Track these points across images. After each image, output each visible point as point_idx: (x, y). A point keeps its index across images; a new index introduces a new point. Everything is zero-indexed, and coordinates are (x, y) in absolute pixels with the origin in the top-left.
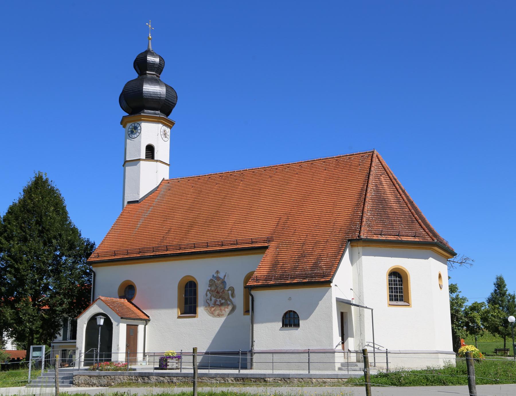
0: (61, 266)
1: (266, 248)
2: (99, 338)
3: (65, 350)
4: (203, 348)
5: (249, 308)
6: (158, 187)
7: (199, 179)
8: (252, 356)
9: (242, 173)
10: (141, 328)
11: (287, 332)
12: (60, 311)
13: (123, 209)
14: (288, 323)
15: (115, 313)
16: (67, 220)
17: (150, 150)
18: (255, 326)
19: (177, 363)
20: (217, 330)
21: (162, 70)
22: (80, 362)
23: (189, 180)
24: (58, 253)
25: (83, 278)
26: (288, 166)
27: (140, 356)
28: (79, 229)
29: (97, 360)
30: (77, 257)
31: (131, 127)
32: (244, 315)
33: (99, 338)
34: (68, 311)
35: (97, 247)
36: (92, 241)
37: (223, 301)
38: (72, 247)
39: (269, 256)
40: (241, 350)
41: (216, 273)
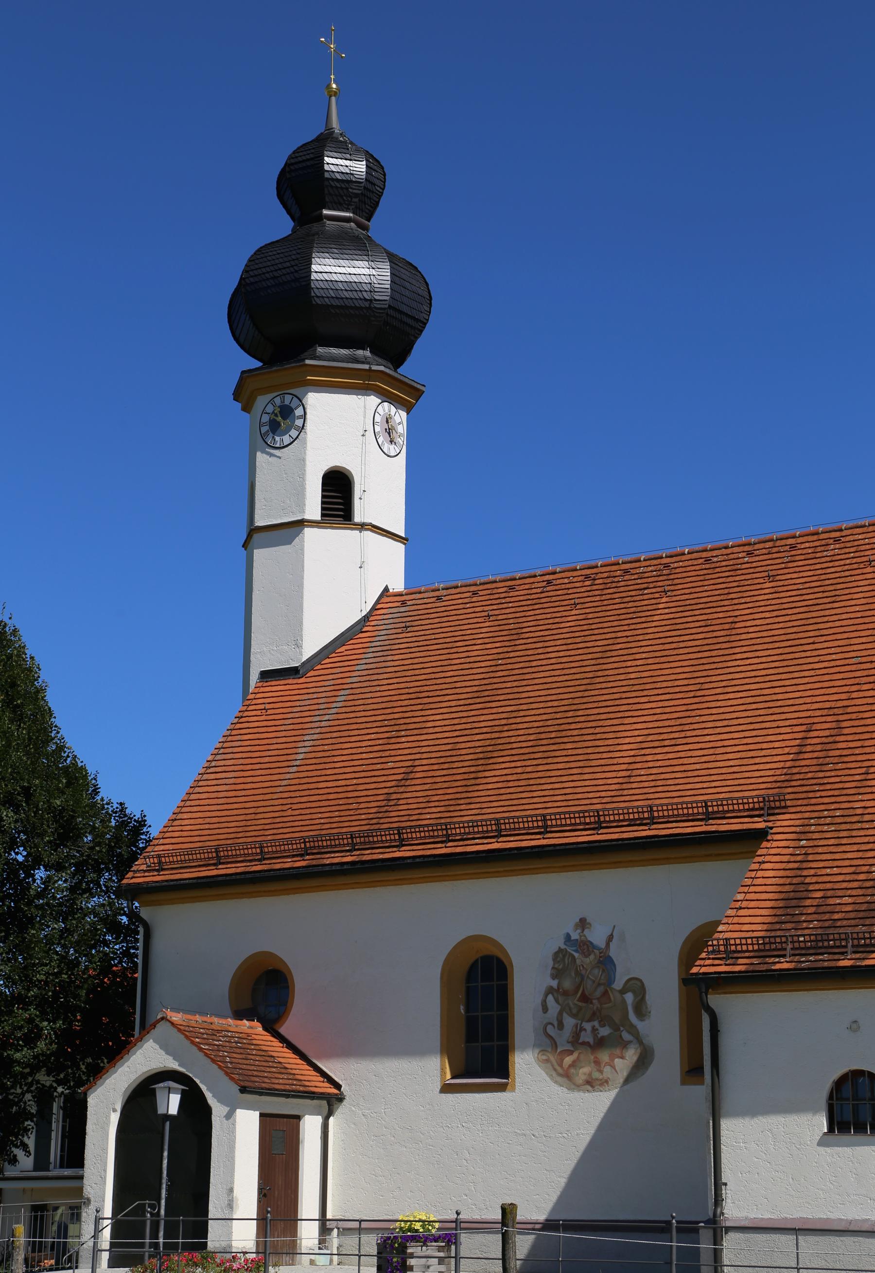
0: (30, 903)
1: (761, 835)
2: (165, 1162)
3: (43, 1208)
4: (535, 1209)
5: (702, 1059)
6: (366, 619)
7: (511, 588)
8: (717, 1240)
9: (667, 566)
10: (311, 1125)
11: (847, 1151)
12: (28, 1065)
13: (244, 699)
14: (849, 1116)
15: (221, 1073)
16: (48, 740)
17: (338, 488)
18: (726, 1125)
19: (441, 1261)
20: (587, 1139)
21: (377, 203)
22: (96, 1251)
23: (475, 593)
24: (20, 858)
25: (106, 943)
26: (837, 535)
27: (308, 1233)
28: (91, 770)
29: (156, 1246)
30: (86, 868)
31: (270, 409)
32: (683, 1083)
33: (165, 1162)
34: (54, 1064)
35: (154, 832)
36: (134, 810)
37: (604, 1031)
38: (68, 833)
39: (770, 866)
40: (676, 1217)
41: (576, 926)
